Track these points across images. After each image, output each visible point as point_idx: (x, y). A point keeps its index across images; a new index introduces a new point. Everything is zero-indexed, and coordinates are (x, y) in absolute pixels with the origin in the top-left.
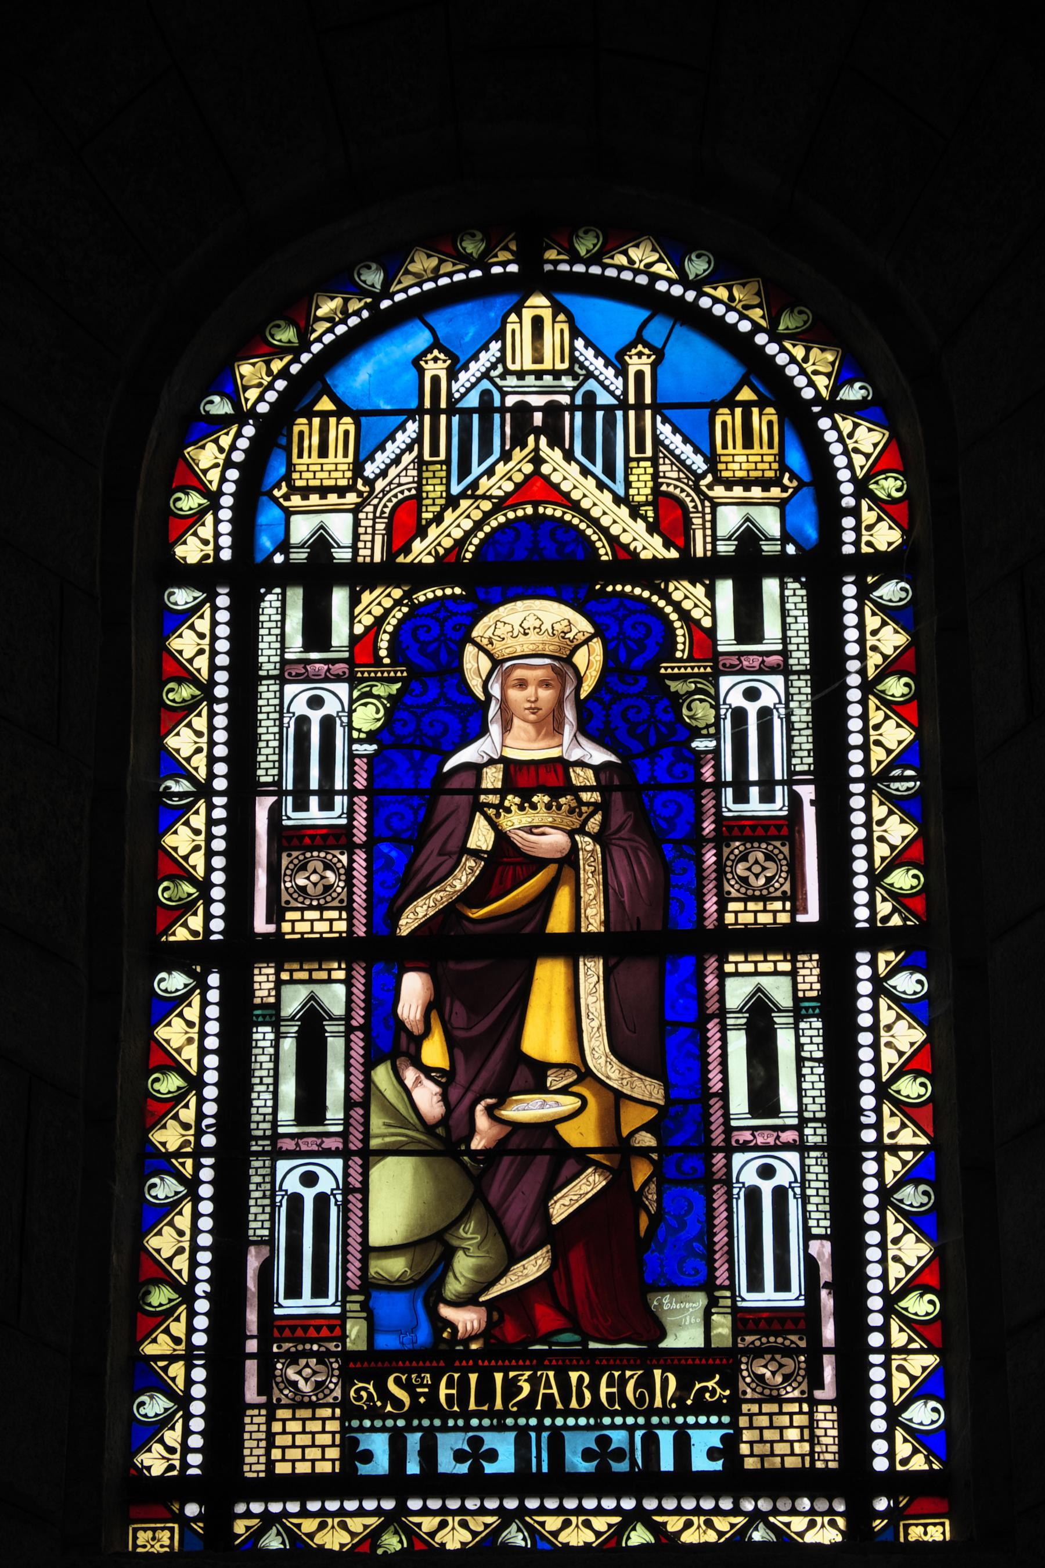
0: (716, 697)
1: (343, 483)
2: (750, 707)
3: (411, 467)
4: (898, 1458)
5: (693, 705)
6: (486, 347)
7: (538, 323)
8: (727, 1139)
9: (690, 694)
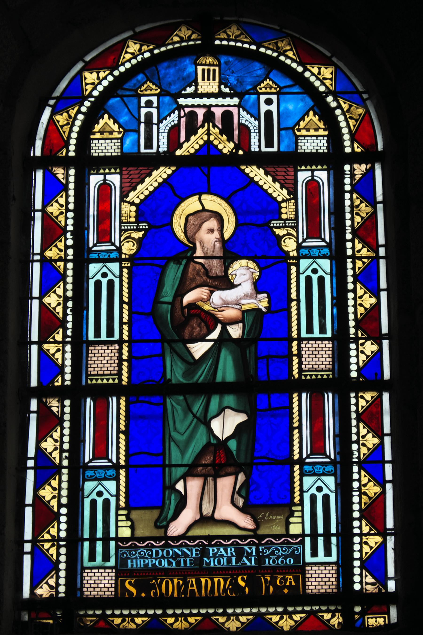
5: (286, 241)
9: (284, 235)
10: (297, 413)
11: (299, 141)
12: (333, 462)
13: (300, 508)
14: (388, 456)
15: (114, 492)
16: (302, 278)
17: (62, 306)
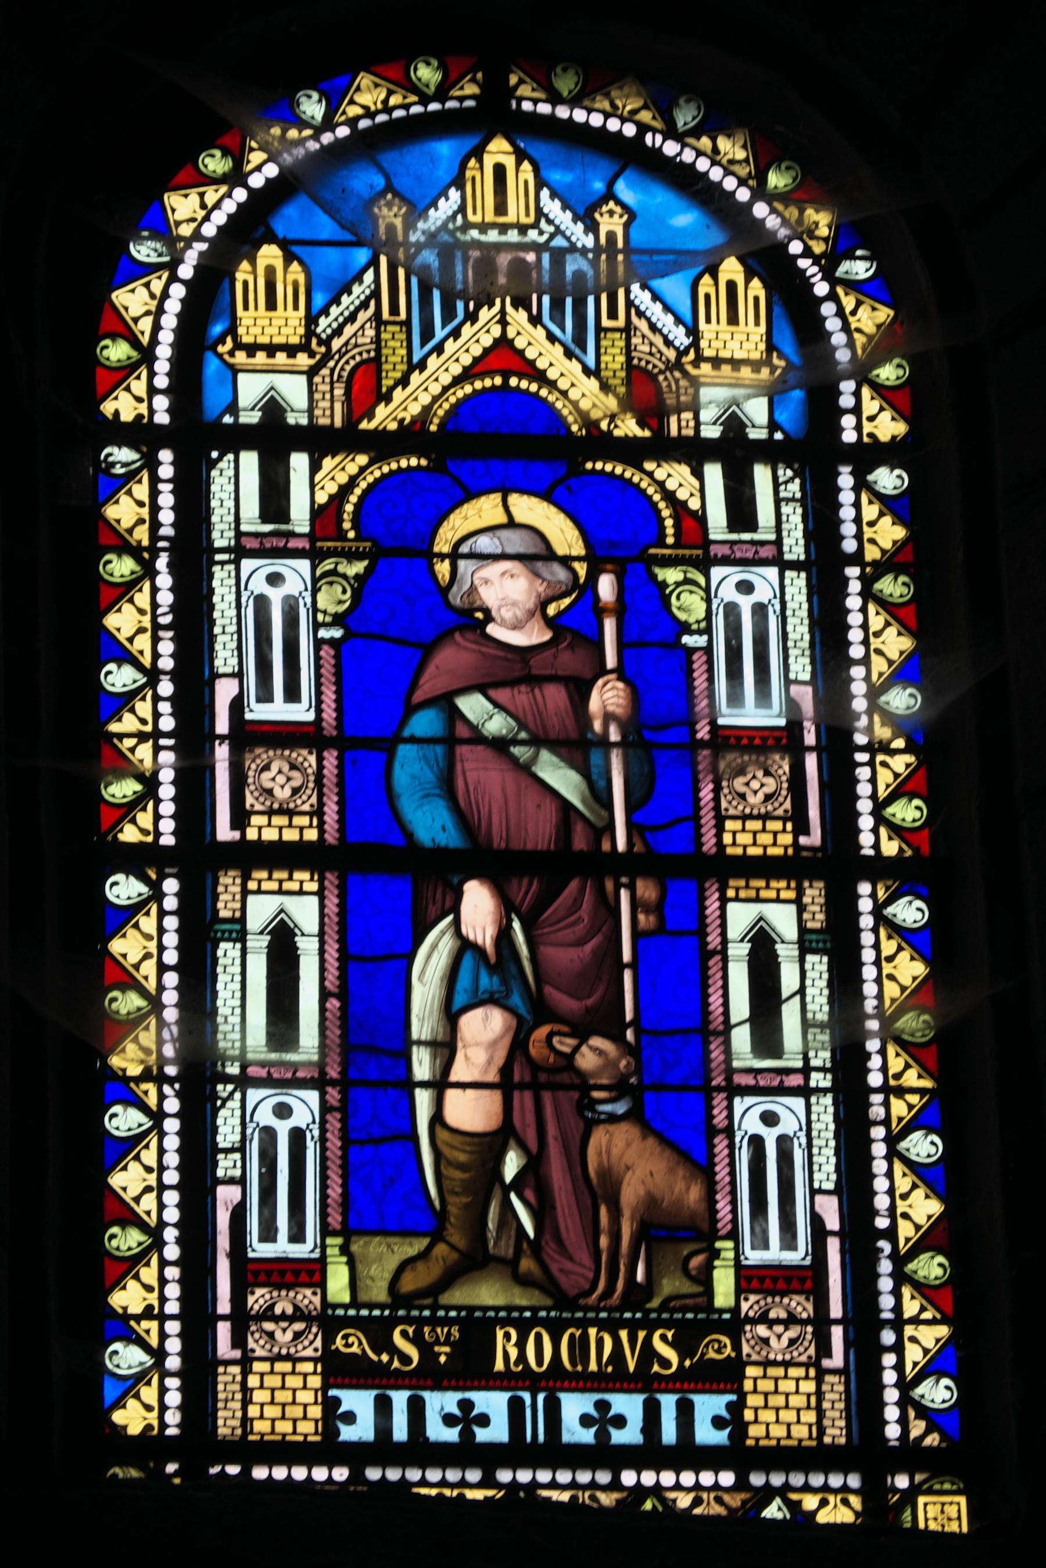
0: (707, 590)
1: (295, 340)
2: (743, 602)
3: (368, 325)
4: (891, 1073)
5: (683, 596)
7: (500, 171)
8: (729, 1079)
17: (147, 525)
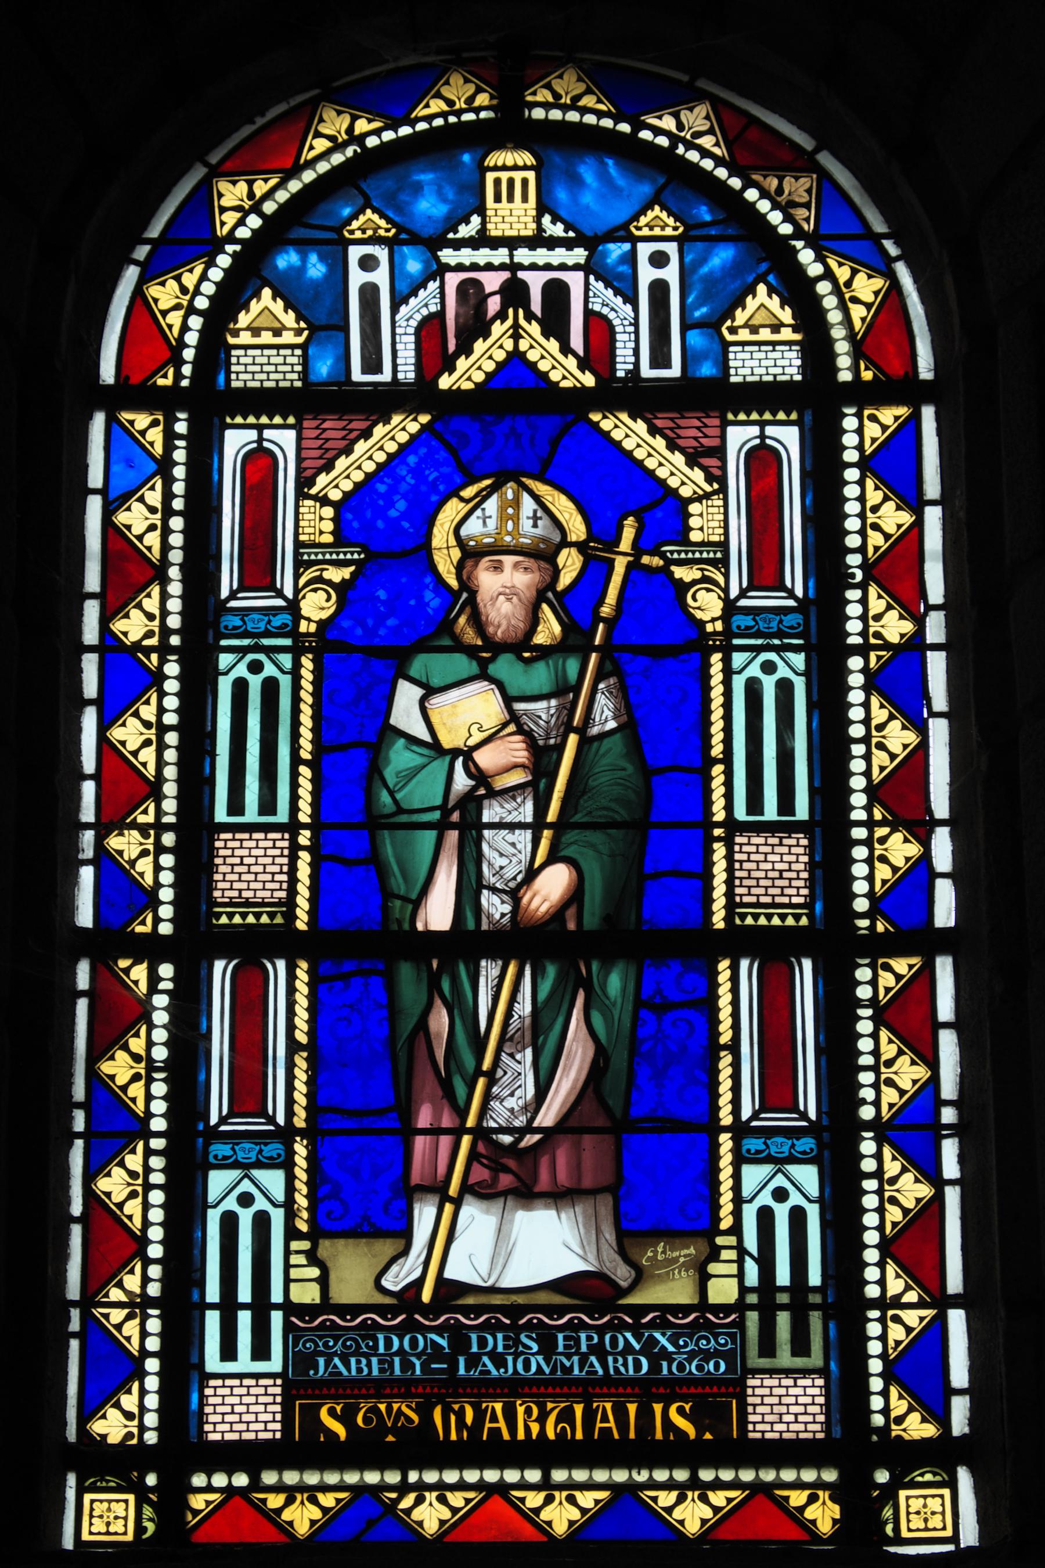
5: (699, 595)
6: (424, 285)
9: (695, 582)
10: (729, 1096)
11: (731, 356)
12: (813, 1129)
13: (732, 1240)
14: (945, 1008)
15: (280, 1196)
16: (739, 684)
17: (161, 428)
